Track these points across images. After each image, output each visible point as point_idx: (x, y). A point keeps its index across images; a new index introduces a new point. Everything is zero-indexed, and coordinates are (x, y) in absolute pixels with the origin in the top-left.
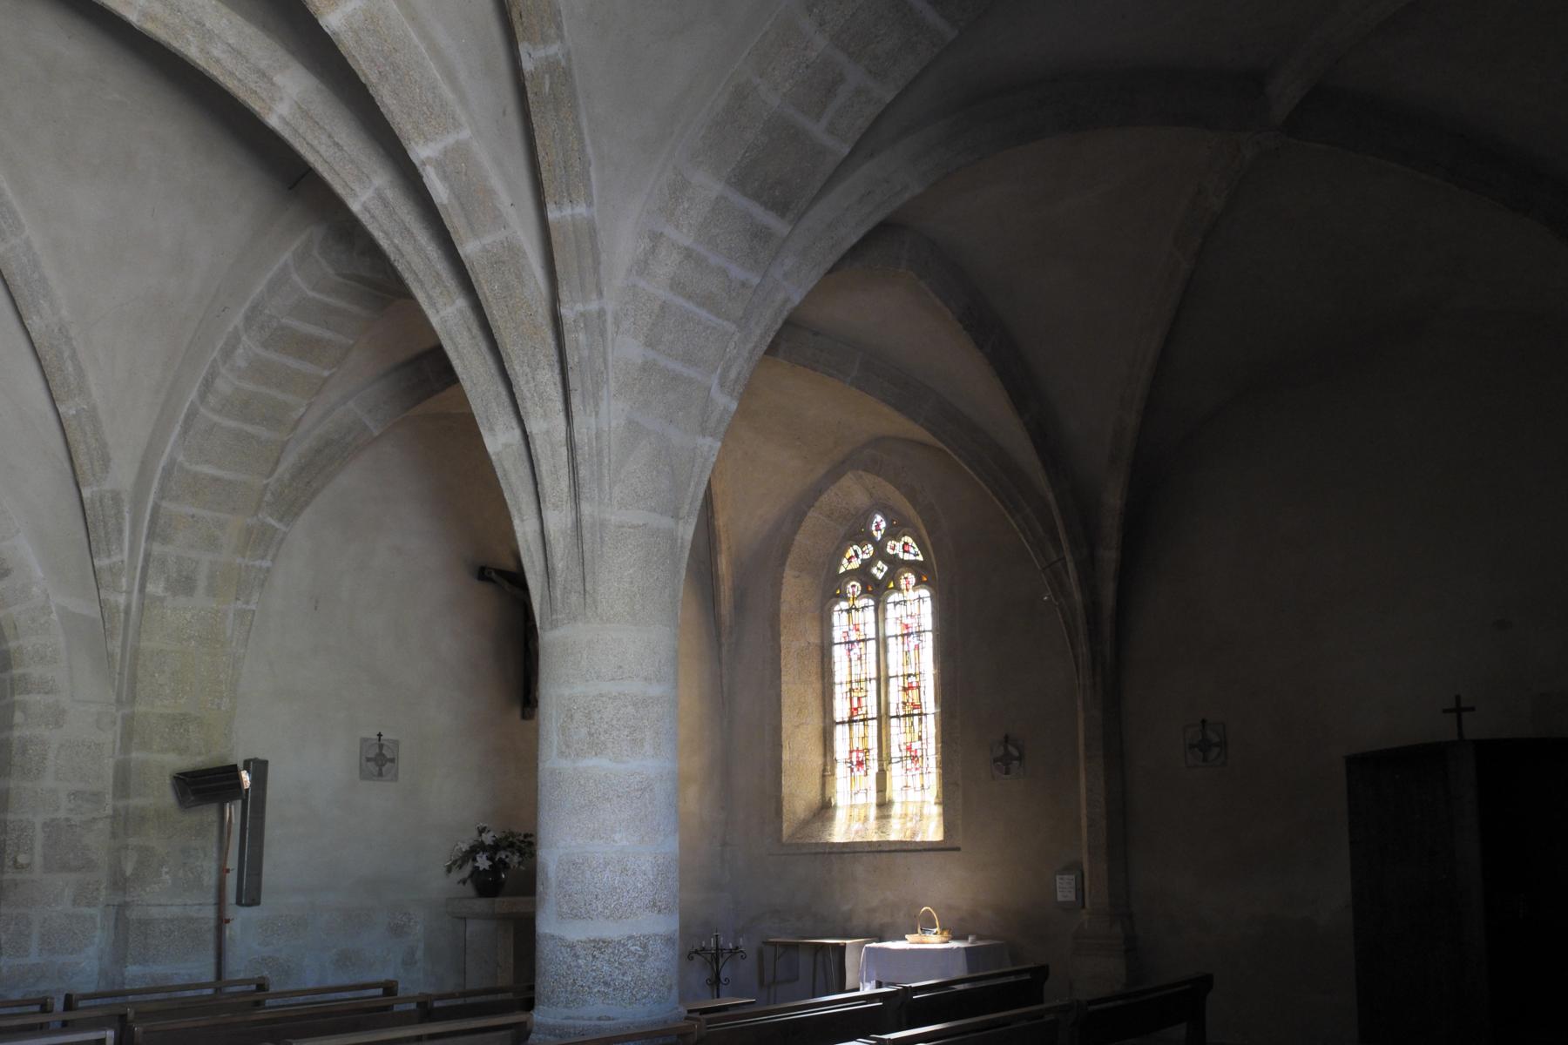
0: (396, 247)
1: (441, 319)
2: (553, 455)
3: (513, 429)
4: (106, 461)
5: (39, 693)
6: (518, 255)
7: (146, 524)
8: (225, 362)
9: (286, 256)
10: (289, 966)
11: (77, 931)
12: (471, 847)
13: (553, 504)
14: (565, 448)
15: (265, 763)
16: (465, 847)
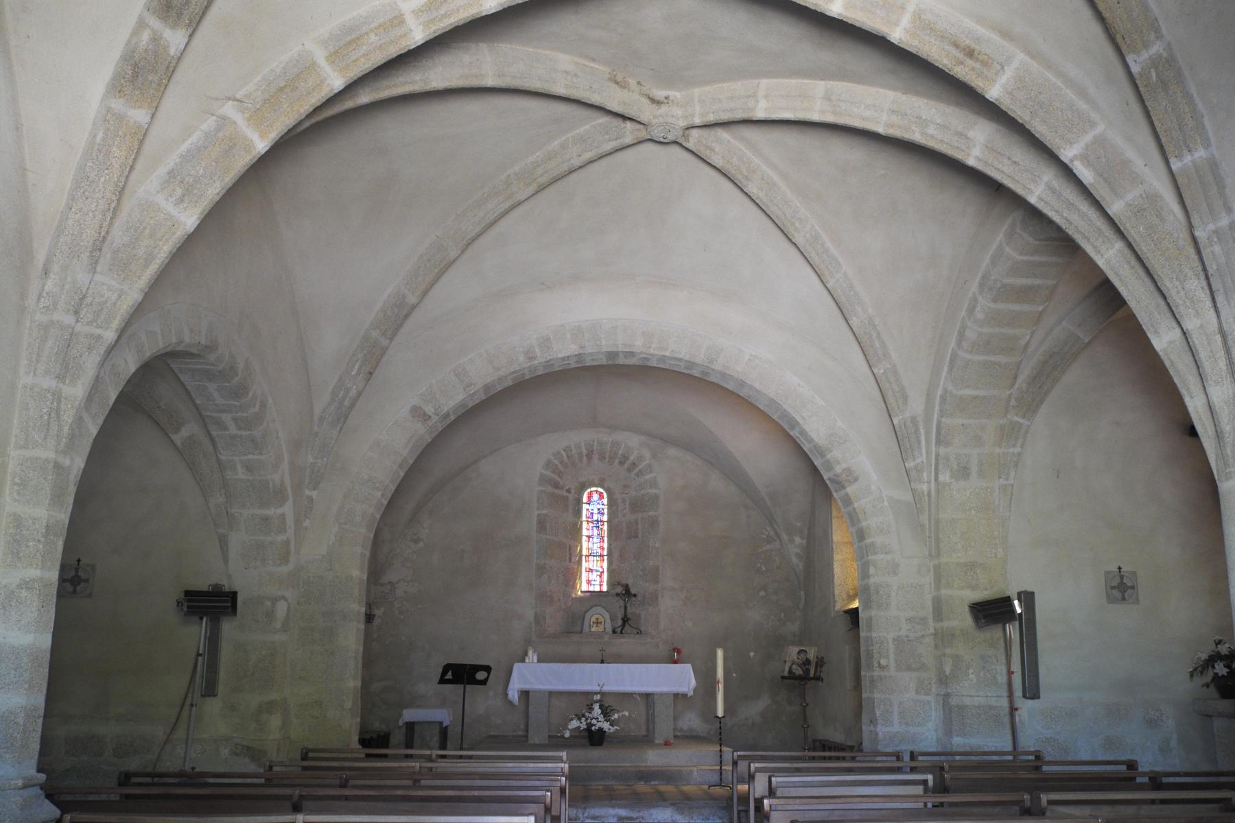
0: (1066, 219)
1: (1106, 261)
2: (1209, 343)
3: (1174, 329)
4: (905, 398)
5: (882, 554)
6: (1156, 200)
7: (934, 435)
8: (970, 318)
9: (1000, 237)
10: (1066, 746)
11: (920, 712)
12: (1209, 657)
13: (1215, 381)
14: (1219, 335)
15: (1032, 594)
16: (1204, 656)
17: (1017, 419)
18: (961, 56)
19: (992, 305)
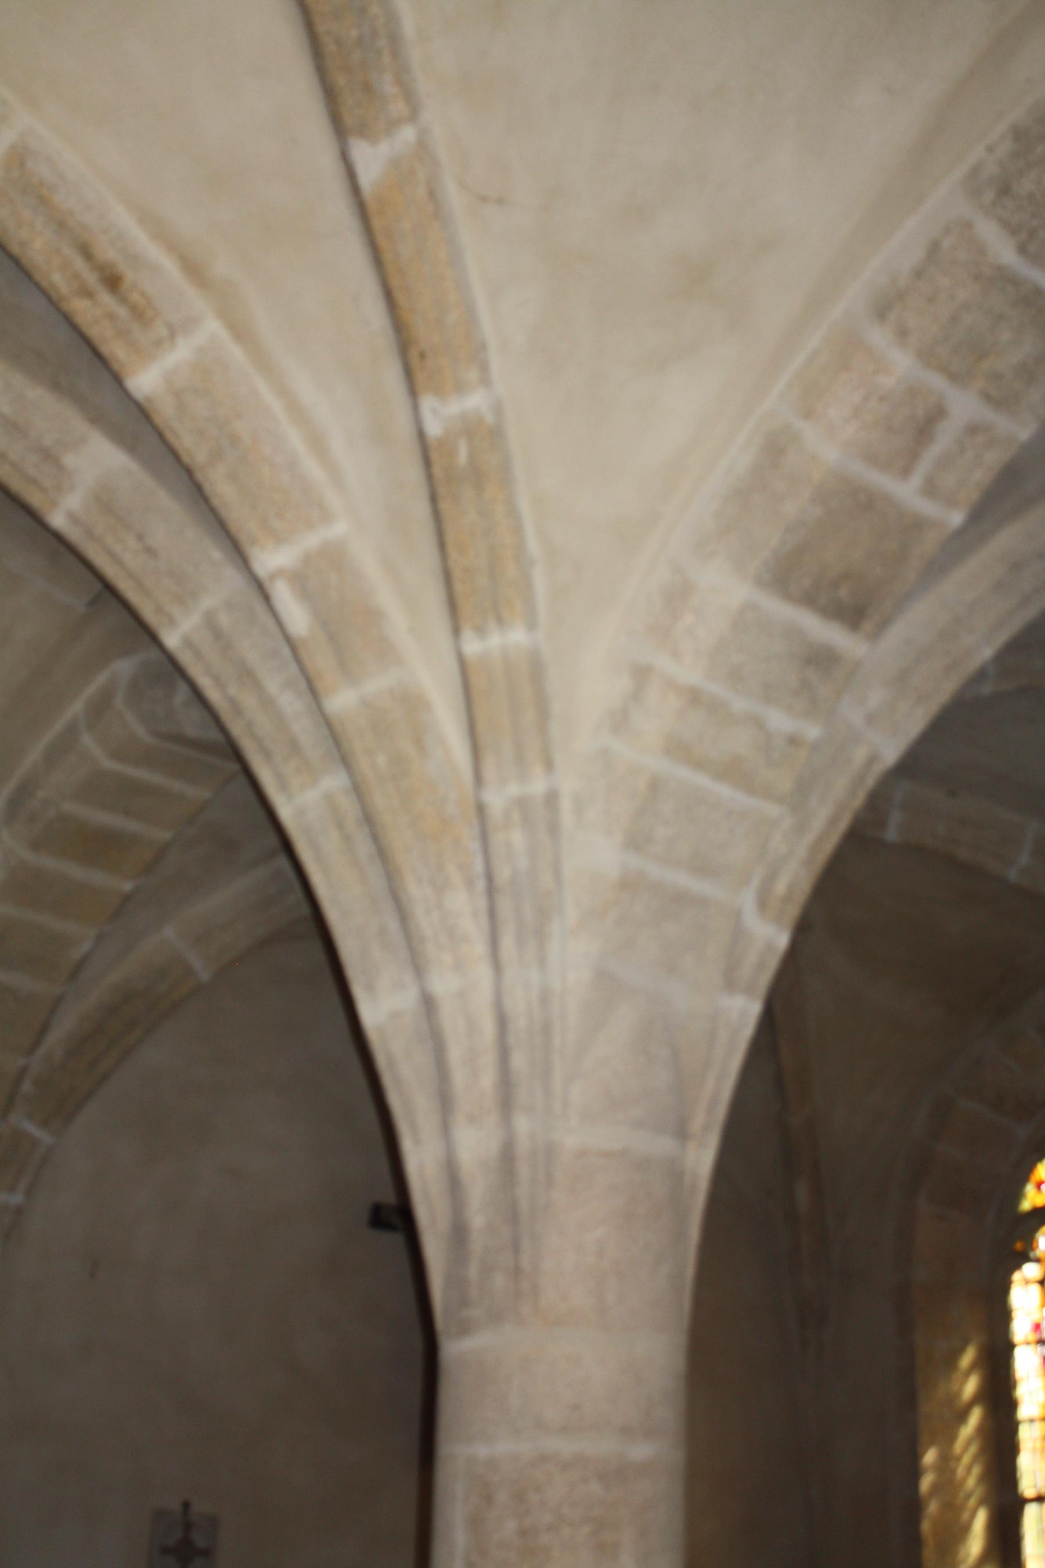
17: (30, 1128)
18: (91, 278)
19: (29, 856)
